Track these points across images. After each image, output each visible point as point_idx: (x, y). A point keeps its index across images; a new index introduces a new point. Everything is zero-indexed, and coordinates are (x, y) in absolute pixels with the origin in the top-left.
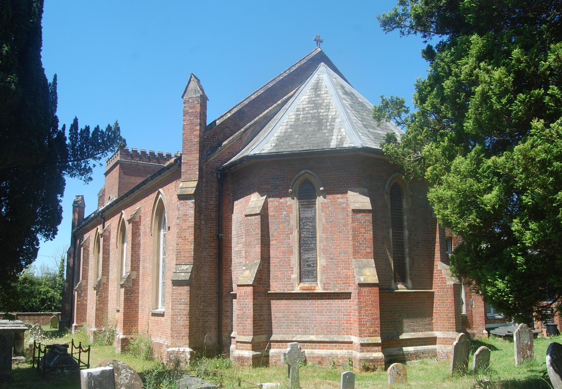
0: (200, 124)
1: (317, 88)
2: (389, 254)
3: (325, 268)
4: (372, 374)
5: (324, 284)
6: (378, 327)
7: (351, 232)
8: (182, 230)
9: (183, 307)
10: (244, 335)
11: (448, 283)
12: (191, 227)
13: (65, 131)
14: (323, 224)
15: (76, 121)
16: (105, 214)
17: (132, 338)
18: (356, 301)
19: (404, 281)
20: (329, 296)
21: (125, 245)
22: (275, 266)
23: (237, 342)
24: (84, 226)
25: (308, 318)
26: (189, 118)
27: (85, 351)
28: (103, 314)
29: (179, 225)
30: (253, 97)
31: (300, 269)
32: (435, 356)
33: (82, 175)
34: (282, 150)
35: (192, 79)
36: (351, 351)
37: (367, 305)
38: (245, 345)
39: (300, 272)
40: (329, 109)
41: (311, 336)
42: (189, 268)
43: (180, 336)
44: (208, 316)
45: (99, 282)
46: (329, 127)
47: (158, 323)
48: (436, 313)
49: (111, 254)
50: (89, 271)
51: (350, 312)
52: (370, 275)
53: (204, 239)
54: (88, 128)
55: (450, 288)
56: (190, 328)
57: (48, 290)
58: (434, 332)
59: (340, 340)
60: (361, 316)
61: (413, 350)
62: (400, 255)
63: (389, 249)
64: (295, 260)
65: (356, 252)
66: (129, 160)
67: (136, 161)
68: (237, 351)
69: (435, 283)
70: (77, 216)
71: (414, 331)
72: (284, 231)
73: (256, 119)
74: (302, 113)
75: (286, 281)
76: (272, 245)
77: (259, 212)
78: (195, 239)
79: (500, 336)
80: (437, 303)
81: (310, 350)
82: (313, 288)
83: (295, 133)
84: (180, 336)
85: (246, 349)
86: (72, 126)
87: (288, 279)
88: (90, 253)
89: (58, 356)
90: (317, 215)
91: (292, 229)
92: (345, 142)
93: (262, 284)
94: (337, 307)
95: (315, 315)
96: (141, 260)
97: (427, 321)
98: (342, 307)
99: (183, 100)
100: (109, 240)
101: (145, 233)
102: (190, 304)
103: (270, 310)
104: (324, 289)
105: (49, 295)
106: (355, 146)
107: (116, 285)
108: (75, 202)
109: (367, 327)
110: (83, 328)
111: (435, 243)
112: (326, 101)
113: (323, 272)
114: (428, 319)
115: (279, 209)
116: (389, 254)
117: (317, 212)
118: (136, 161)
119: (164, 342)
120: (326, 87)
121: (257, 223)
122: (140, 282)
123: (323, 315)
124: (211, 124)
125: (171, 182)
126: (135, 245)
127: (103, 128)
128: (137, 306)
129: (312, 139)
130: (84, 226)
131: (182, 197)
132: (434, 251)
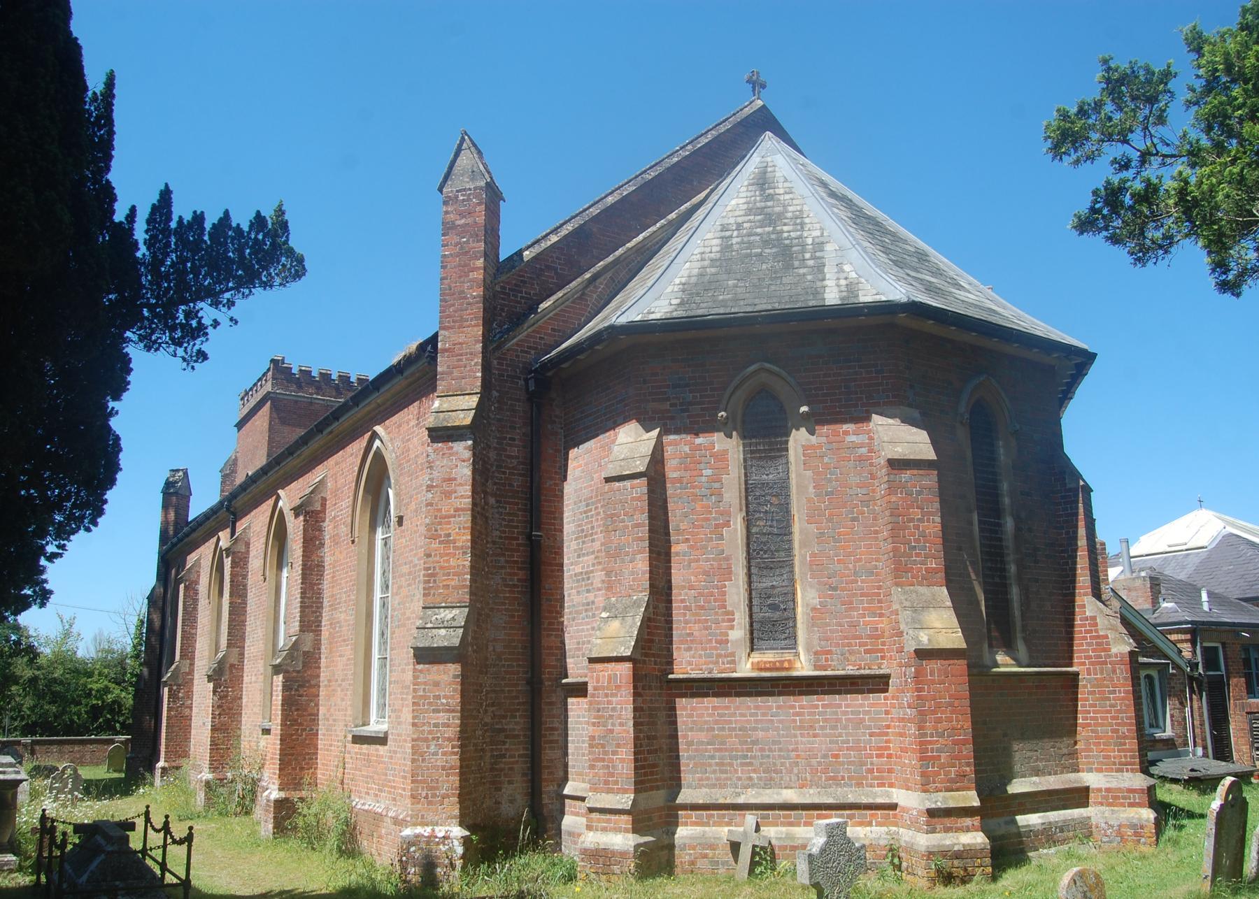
0: (486, 255)
1: (763, 181)
2: (973, 576)
3: (817, 614)
4: (960, 891)
5: (816, 653)
6: (968, 765)
7: (885, 518)
8: (440, 519)
9: (442, 717)
10: (609, 791)
11: (1114, 650)
12: (463, 510)
13: (136, 226)
14: (809, 500)
15: (166, 195)
16: (238, 503)
17: (302, 799)
18: (907, 698)
19: (1009, 647)
20: (830, 685)
21: (285, 573)
22: (686, 608)
23: (591, 810)
24: (187, 535)
25: (774, 742)
26: (456, 239)
27: (180, 842)
28: (228, 738)
29: (430, 504)
30: (610, 200)
31: (751, 616)
32: (1089, 835)
33: (178, 343)
34: (700, 312)
35: (465, 146)
36: (894, 829)
37: (938, 706)
38: (613, 817)
39: (751, 625)
40: (802, 224)
41: (785, 791)
42: (459, 615)
43: (434, 796)
44: (504, 743)
45: (221, 663)
46: (811, 263)
47: (369, 761)
48: (1084, 726)
49: (250, 595)
50: (198, 639)
51: (888, 727)
52: (942, 627)
53: (494, 543)
54: (199, 219)
55: (1121, 662)
56: (461, 774)
57: (107, 687)
58: (1081, 774)
59: (864, 800)
60: (925, 735)
61: (1040, 821)
62: (997, 580)
63: (973, 563)
64: (738, 594)
65: (901, 571)
66: (292, 393)
67: (308, 394)
68: (591, 834)
69: (1081, 651)
70: (172, 516)
71: (1037, 772)
72: (708, 519)
73: (618, 253)
74: (735, 233)
75: (716, 649)
76: (677, 554)
77: (642, 469)
78: (473, 541)
79: (1175, 781)
80: (1087, 699)
81: (784, 829)
82: (786, 665)
83: (725, 277)
84: (434, 796)
85: (617, 830)
86: (154, 209)
87: (719, 642)
88: (200, 596)
89: (103, 856)
90: (793, 476)
91: (729, 514)
92: (861, 293)
93: (653, 655)
94: (852, 713)
95: (795, 736)
96: (326, 604)
97: (1063, 745)
98: (866, 713)
99: (441, 198)
100: (246, 563)
101: (335, 538)
102: (462, 710)
103: (673, 723)
104: (816, 668)
105: (110, 698)
106: (891, 298)
107: (262, 670)
108: (169, 484)
109: (942, 766)
110: (181, 771)
111: (1076, 550)
112: (790, 209)
113: (813, 622)
114: (1067, 741)
115: (691, 463)
116: (973, 576)
117: (792, 468)
118: (308, 394)
119: (388, 809)
120: (786, 180)
121: (638, 499)
122: (323, 660)
123: (815, 736)
124: (510, 258)
125: (407, 406)
126: (311, 569)
127: (243, 219)
128: (314, 718)
129: (773, 288)
130: (187, 535)
131: (441, 434)
132: (1075, 569)
